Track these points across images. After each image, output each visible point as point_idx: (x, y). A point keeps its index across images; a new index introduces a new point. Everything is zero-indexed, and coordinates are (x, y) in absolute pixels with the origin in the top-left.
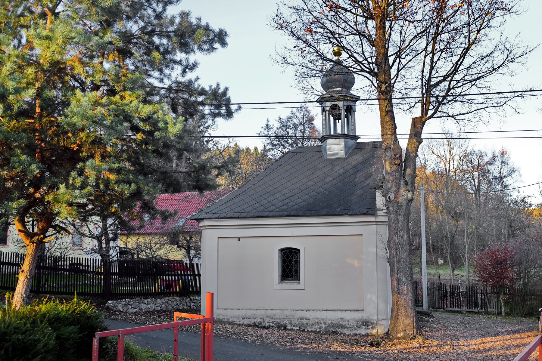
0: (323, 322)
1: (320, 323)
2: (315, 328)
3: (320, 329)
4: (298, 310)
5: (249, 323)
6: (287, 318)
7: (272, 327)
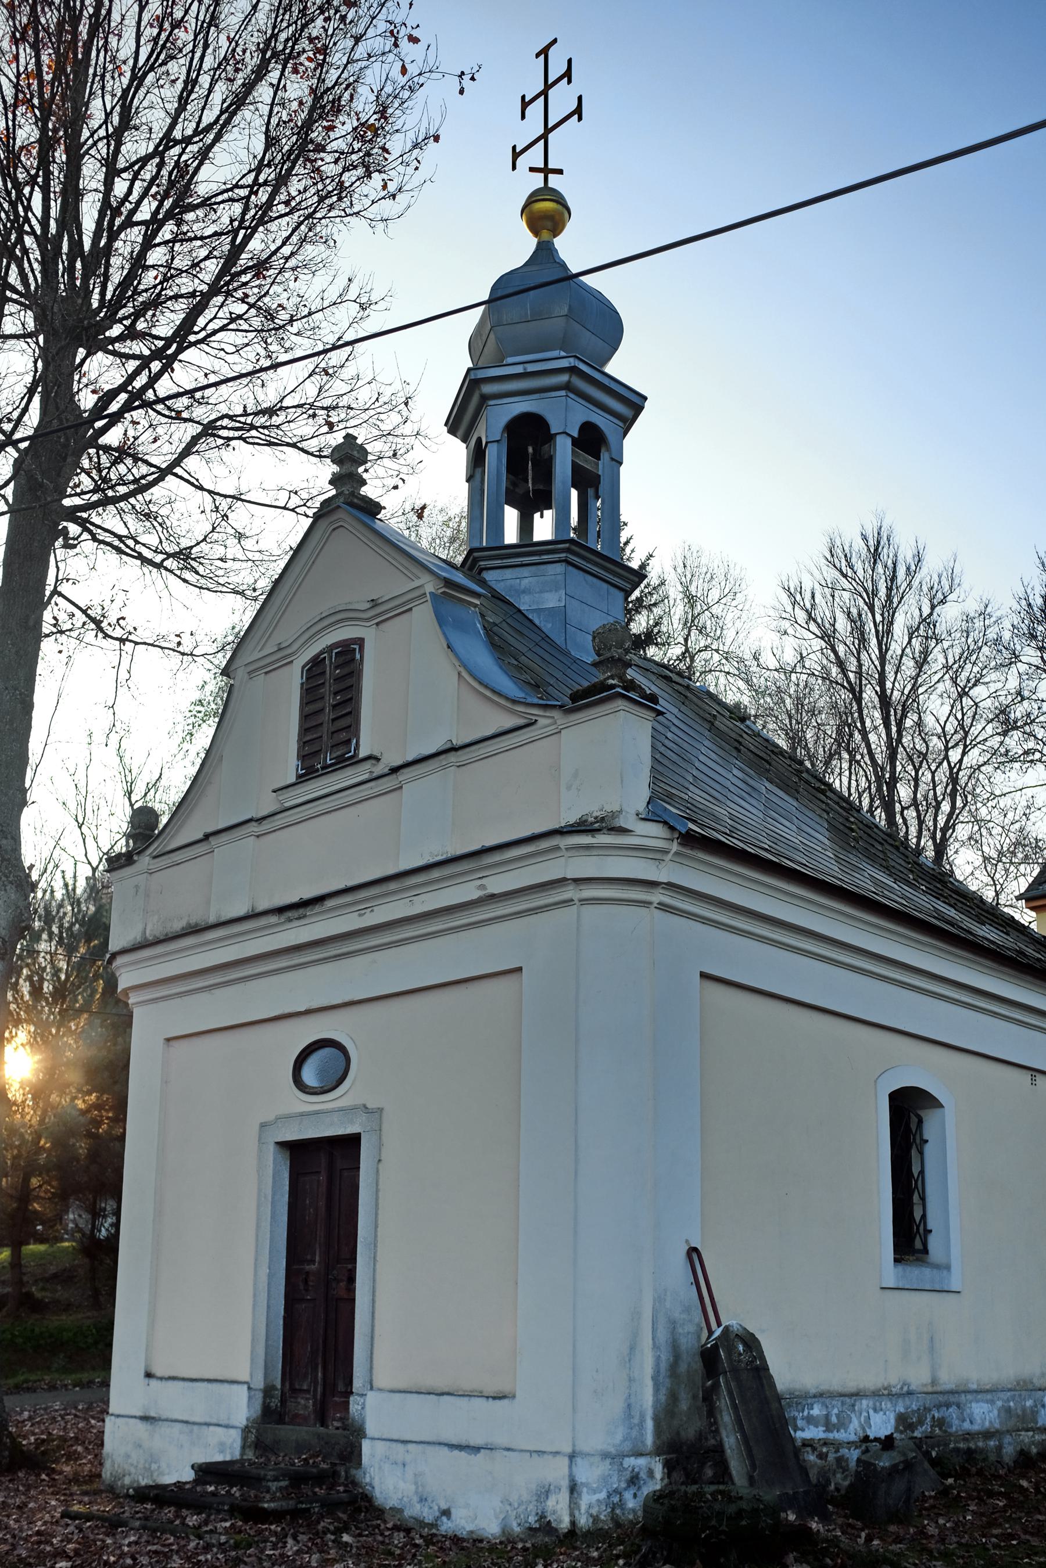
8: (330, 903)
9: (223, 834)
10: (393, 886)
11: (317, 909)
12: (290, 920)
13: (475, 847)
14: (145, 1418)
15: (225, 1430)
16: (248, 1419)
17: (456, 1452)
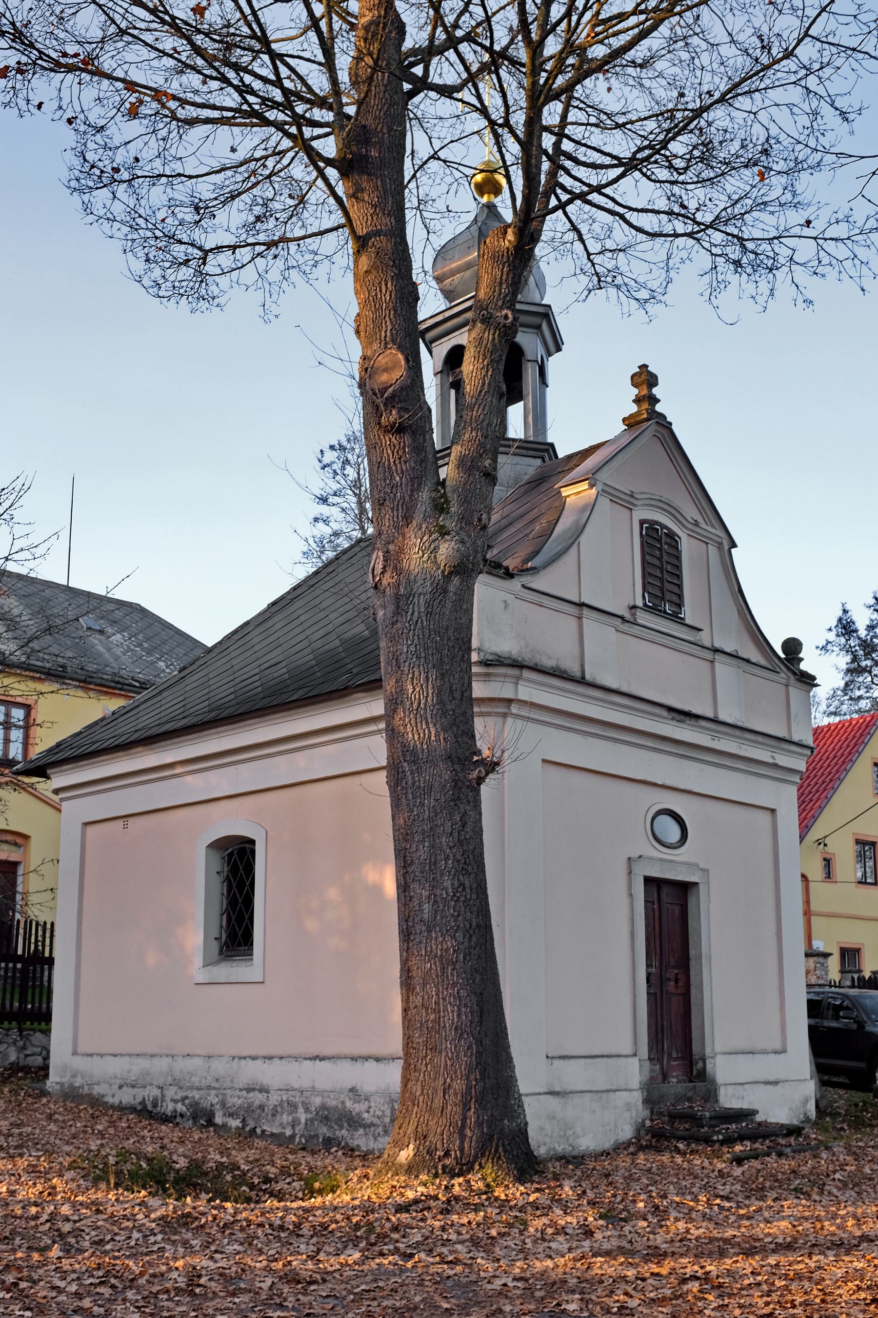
0: (303, 1103)
1: (293, 1107)
2: (281, 1124)
3: (293, 1127)
4: (245, 1058)
5: (132, 1102)
6: (217, 1085)
7: (182, 1116)
8: (704, 723)
9: (596, 612)
10: (738, 733)
11: (693, 722)
12: (673, 719)
13: (686, 708)
14: (551, 1093)
15: (628, 1093)
16: (640, 1083)
17: (768, 1086)
